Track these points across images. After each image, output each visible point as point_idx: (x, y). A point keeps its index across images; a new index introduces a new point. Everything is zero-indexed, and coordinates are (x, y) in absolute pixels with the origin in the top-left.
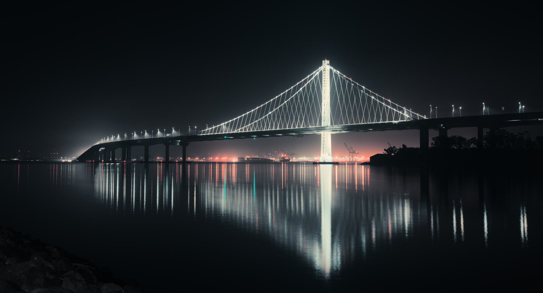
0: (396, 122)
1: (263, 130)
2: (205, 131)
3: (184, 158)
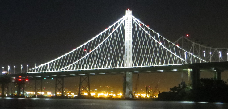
1: (149, 66)
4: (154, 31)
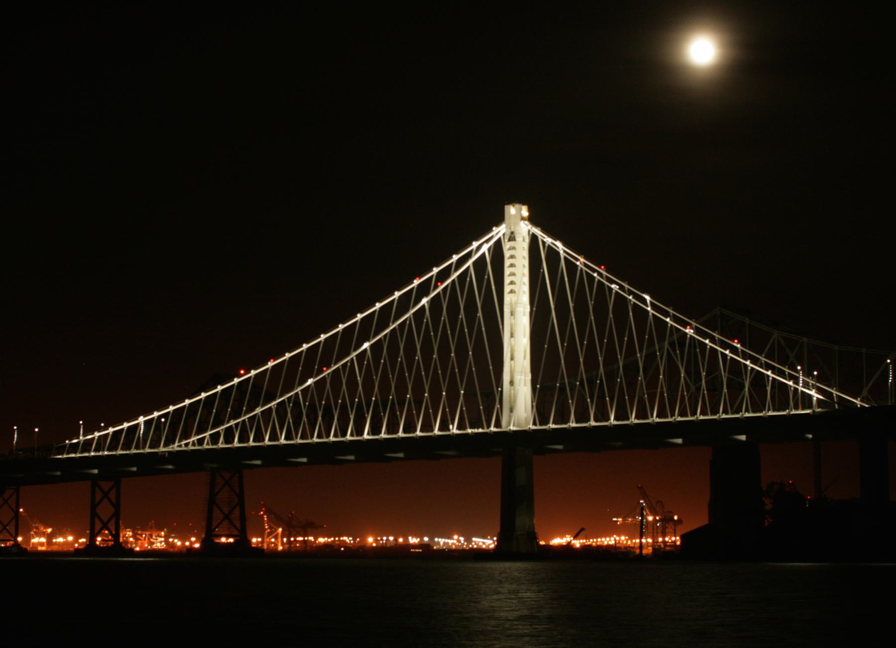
2: (94, 438)
4: (834, 392)
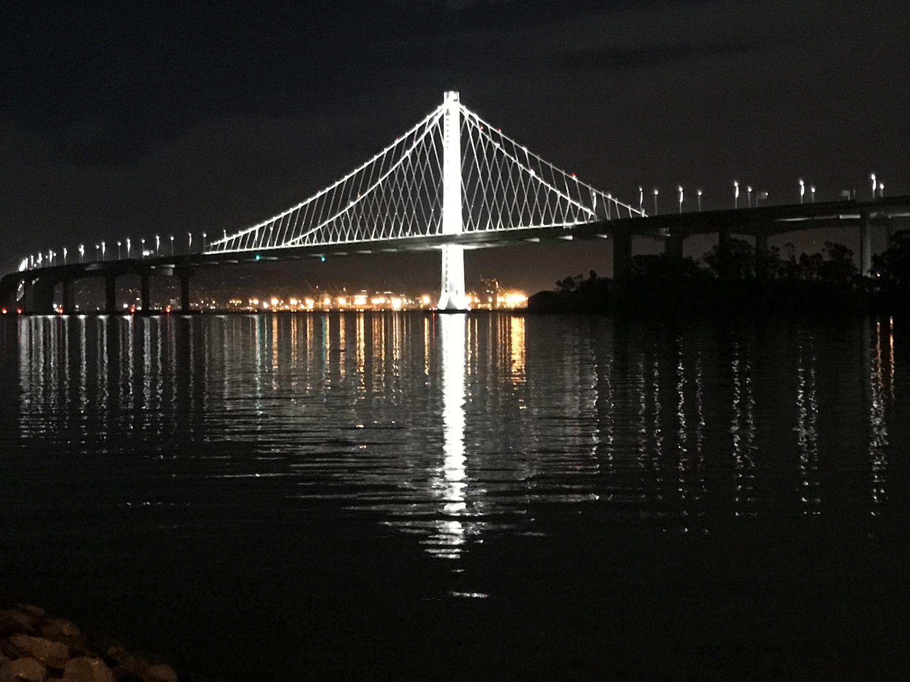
0: (570, 225)
3: (185, 303)
